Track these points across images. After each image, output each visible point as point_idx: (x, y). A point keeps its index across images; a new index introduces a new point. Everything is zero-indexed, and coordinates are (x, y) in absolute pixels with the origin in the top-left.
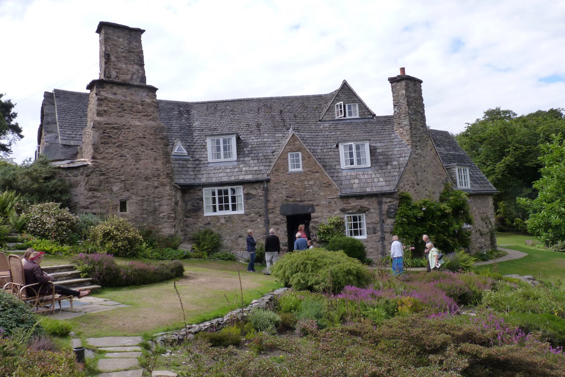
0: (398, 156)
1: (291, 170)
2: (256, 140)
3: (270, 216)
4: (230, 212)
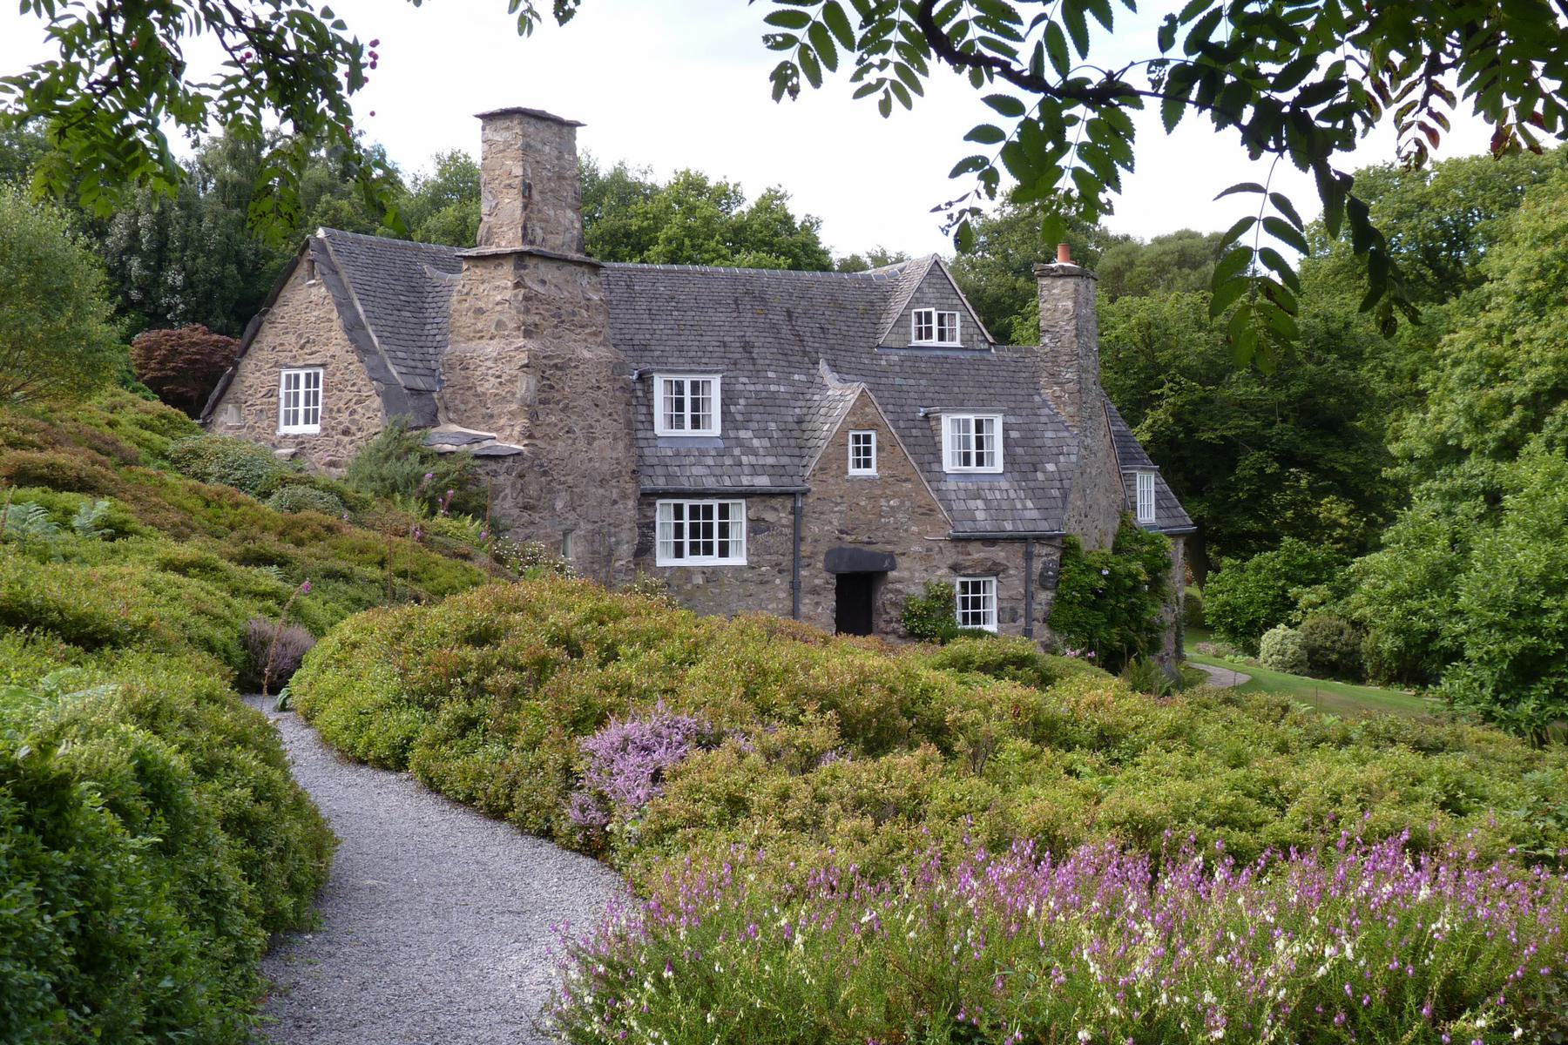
0: (1055, 451)
1: (853, 472)
2: (752, 388)
3: (804, 573)
4: (714, 560)
